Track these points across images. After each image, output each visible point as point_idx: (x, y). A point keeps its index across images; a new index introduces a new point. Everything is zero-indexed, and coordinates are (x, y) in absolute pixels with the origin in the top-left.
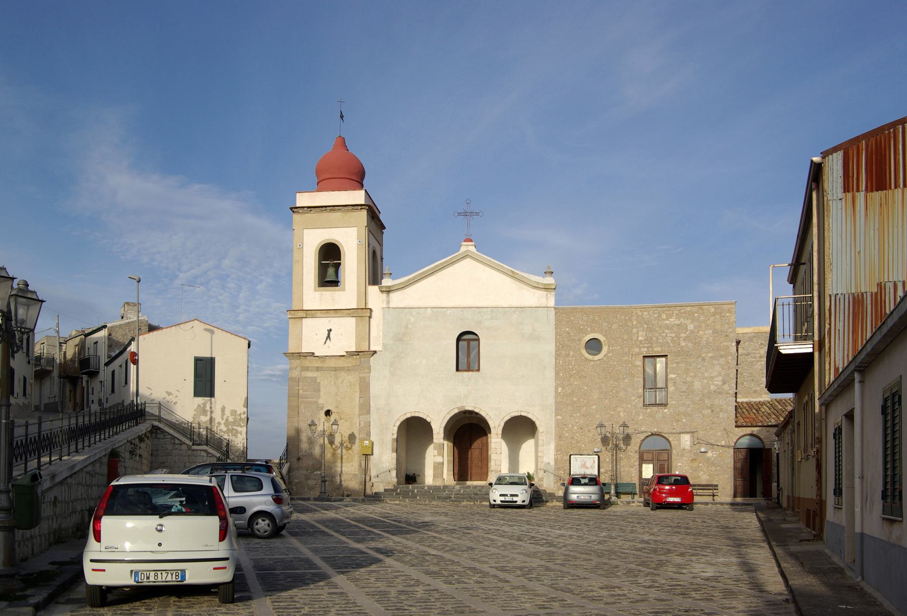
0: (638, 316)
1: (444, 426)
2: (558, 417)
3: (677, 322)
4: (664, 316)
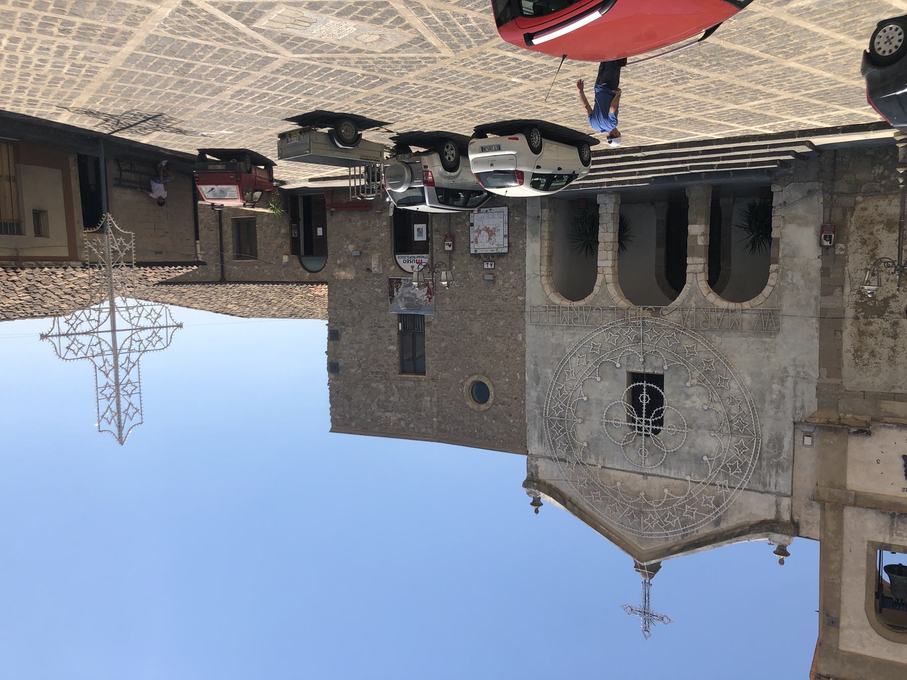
3: (388, 414)
4: (403, 423)
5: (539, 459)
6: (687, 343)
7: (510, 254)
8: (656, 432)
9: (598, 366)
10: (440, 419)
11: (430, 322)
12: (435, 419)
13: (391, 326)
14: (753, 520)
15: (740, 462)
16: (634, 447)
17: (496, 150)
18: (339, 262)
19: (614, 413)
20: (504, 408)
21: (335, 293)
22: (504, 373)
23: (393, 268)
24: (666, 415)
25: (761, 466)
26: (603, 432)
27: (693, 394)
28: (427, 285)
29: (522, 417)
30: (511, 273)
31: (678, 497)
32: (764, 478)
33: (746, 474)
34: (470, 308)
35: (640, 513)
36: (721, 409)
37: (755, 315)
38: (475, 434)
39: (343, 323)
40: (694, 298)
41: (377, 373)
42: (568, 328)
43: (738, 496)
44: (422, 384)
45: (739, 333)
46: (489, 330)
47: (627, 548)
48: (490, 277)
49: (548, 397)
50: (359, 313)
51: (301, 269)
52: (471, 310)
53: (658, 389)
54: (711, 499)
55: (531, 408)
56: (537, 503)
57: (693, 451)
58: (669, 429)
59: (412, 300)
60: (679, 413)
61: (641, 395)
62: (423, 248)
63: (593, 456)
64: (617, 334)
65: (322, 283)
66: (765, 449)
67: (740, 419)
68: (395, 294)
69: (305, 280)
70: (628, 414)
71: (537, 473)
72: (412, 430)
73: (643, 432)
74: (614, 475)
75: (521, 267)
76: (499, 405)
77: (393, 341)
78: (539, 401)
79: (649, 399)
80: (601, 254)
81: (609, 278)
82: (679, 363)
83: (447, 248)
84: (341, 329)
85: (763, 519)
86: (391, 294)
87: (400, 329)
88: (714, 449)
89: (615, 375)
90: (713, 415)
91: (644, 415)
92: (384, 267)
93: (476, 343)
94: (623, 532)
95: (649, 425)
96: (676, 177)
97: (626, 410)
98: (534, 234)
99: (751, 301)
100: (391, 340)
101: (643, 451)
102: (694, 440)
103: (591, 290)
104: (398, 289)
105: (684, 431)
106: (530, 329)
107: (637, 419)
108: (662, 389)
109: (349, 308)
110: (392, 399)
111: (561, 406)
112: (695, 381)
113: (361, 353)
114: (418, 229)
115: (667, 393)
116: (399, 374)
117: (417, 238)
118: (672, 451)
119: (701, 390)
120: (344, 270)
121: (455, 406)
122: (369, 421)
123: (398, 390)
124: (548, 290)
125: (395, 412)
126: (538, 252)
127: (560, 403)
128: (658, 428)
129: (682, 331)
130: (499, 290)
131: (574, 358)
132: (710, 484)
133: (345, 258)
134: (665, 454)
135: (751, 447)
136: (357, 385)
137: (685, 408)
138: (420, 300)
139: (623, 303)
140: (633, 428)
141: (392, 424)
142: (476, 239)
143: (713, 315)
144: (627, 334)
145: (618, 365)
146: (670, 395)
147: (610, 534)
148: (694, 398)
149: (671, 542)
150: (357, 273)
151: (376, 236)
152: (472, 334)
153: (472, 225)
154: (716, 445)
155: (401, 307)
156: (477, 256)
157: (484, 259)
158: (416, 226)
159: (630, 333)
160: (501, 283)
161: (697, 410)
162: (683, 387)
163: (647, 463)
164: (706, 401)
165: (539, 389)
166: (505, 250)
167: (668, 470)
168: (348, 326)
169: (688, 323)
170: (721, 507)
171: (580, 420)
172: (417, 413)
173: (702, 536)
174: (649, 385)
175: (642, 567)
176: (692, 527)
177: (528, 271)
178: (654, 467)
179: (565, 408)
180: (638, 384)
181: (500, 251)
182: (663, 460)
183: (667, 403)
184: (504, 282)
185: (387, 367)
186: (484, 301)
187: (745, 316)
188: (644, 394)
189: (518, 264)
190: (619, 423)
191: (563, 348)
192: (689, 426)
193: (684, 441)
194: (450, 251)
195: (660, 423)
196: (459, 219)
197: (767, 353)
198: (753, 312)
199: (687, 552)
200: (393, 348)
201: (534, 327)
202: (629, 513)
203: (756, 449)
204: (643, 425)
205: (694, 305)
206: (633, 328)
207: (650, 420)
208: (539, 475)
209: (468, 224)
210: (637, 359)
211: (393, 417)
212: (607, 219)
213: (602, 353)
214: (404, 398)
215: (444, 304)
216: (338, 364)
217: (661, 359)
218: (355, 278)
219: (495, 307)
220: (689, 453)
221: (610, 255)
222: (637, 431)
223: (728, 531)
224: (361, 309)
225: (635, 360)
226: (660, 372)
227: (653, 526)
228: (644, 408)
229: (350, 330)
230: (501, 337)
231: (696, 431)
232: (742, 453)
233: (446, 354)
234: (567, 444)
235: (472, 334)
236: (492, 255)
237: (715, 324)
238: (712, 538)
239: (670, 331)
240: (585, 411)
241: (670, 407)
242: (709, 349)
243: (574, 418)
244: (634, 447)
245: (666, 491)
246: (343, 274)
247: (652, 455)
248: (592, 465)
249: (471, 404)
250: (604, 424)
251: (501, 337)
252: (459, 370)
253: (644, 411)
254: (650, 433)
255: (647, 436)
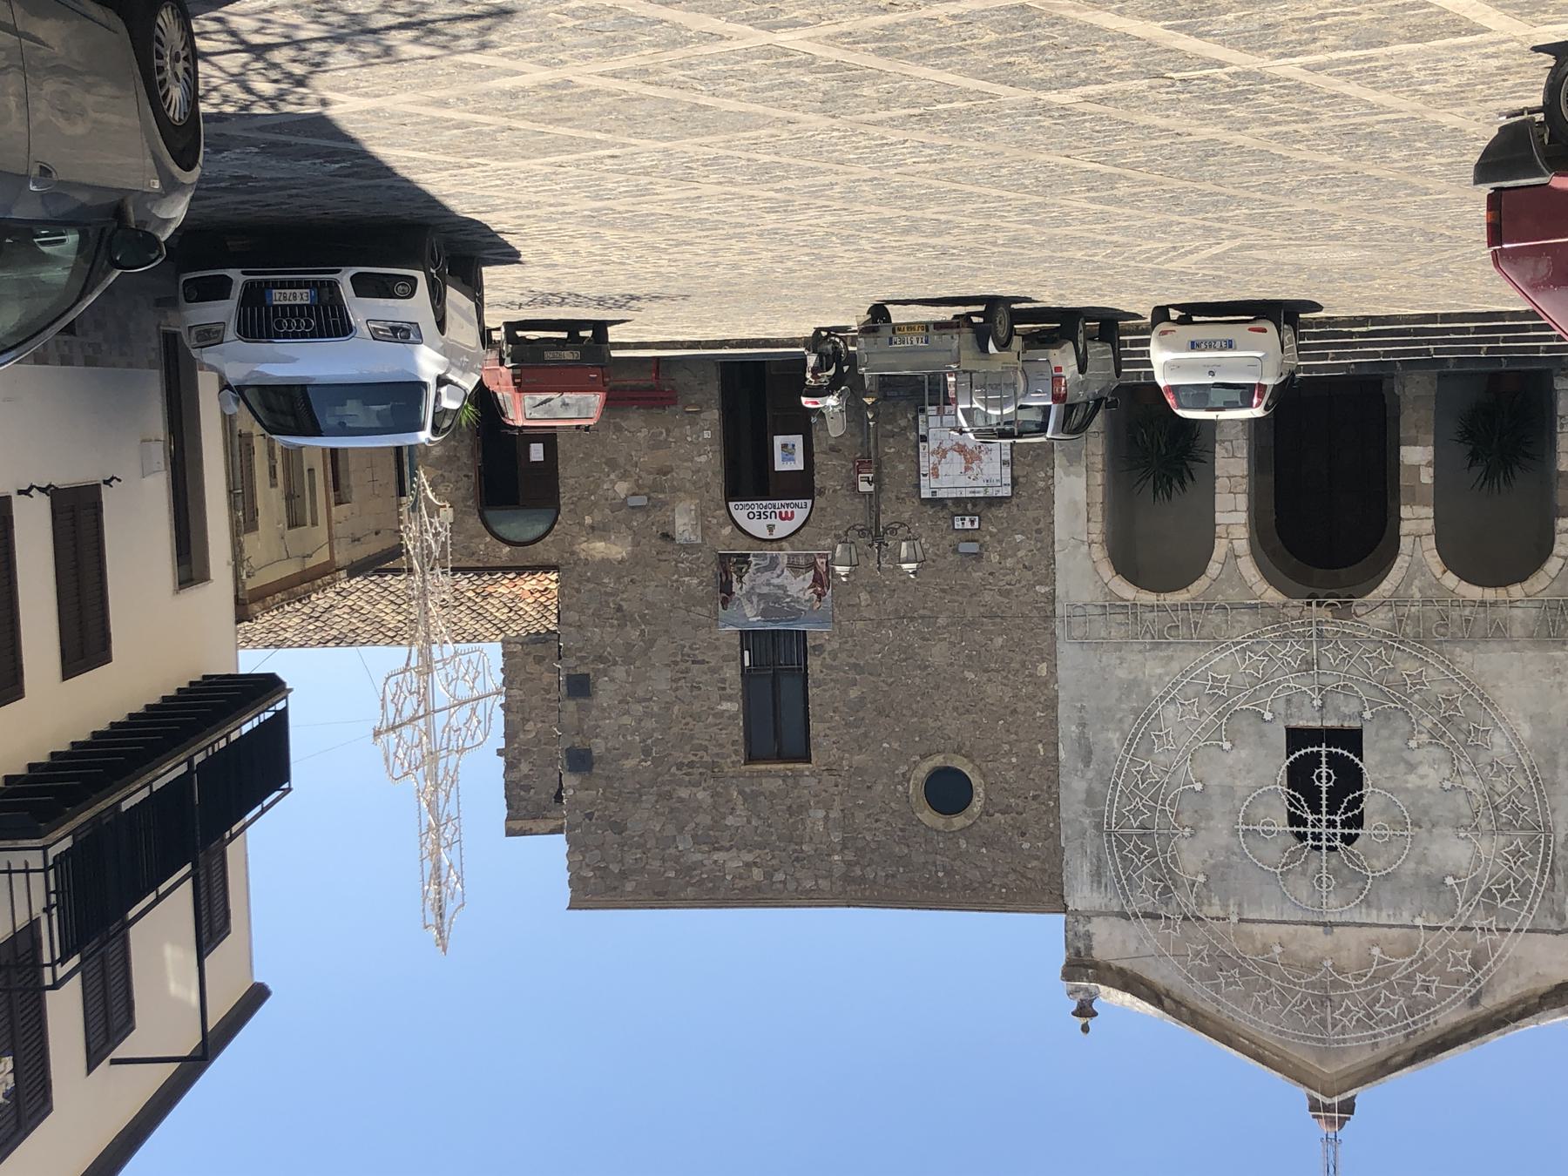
0: (829, 876)
1: (1398, 560)
2: (1047, 589)
3: (719, 856)
4: (757, 874)
5: (1095, 920)
6: (1408, 667)
7: (1014, 501)
8: (1349, 840)
9: (1224, 720)
10: (850, 856)
11: (822, 645)
12: (836, 858)
13: (725, 659)
14: (1544, 986)
15: (1516, 881)
16: (1304, 873)
17: (1221, 349)
18: (588, 520)
19: (1261, 811)
20: (1009, 819)
21: (578, 591)
22: (1006, 747)
23: (727, 530)
24: (1368, 806)
25: (1554, 885)
26: (1237, 850)
27: (1421, 762)
28: (813, 565)
29: (1054, 835)
30: (1019, 537)
31: (1401, 960)
32: (1559, 906)
33: (1528, 902)
34: (921, 612)
35: (1323, 1001)
36: (1477, 787)
37: (1534, 611)
38: (939, 882)
39: (601, 658)
40: (1416, 582)
41: (691, 765)
42: (1156, 646)
43: (1512, 945)
44: (804, 782)
45: (1505, 645)
46: (970, 657)
47: (1299, 1076)
48: (973, 548)
49: (1114, 789)
50: (643, 631)
51: (488, 539)
52: (922, 617)
53: (1352, 756)
54: (1464, 957)
55: (1073, 816)
56: (1085, 1010)
57: (1423, 869)
58: (1376, 832)
59: (778, 599)
60: (1394, 799)
61: (1317, 771)
62: (800, 486)
63: (1215, 900)
64: (1265, 655)
65: (546, 568)
66: (1558, 849)
67: (1514, 802)
68: (736, 587)
69: (497, 563)
70: (1292, 809)
71: (1089, 948)
72: (780, 886)
73: (1324, 843)
74: (1262, 934)
75: (1041, 525)
76: (997, 815)
77: (728, 691)
78: (1091, 798)
79: (1334, 778)
80: (1222, 500)
81: (1242, 546)
82: (1393, 705)
83: (864, 487)
84: (596, 671)
85: (1560, 982)
86: (726, 588)
87: (747, 663)
88: (1465, 864)
89: (1262, 735)
90: (1461, 798)
91: (1324, 809)
92: (705, 529)
93: (937, 687)
94: (1284, 1043)
95: (1335, 827)
96: (1398, 365)
97: (1287, 803)
98: (1073, 459)
99: (1526, 584)
100: (724, 689)
101: (1324, 879)
102: (1426, 848)
103: (1200, 571)
104: (741, 577)
105: (1405, 833)
106: (1068, 653)
107: (1310, 818)
108: (1360, 755)
109: (616, 622)
110: (730, 821)
111: (1143, 805)
112: (1425, 738)
113: (650, 724)
114: (784, 446)
115: (1370, 764)
116: (745, 764)
117: (780, 465)
118: (1384, 873)
119: (1437, 753)
120: (602, 539)
121: (888, 824)
122: (672, 874)
123: (745, 800)
124: (1107, 571)
125: (739, 850)
126: (1081, 495)
127: (1141, 799)
128: (1353, 831)
129: (1396, 645)
130: (991, 574)
131: (1172, 708)
132: (1462, 929)
133: (607, 511)
134: (1370, 881)
135: (1535, 852)
136: (641, 796)
137: (1407, 790)
138: (797, 601)
139: (1272, 595)
140: (1301, 837)
141: (729, 877)
142: (935, 468)
143: (1455, 614)
144: (1285, 655)
145: (1268, 716)
146: (1377, 766)
147: (1261, 1051)
148: (1423, 770)
149: (1383, 1051)
150: (636, 544)
151: (686, 461)
152: (926, 667)
153: (924, 439)
154: (1469, 853)
155: (752, 616)
156: (936, 502)
157: (953, 509)
158: (778, 440)
159: (1290, 651)
160: (995, 558)
161: (1430, 791)
162: (1402, 750)
163: (1333, 901)
164: (1447, 773)
165: (1090, 774)
166: (1007, 491)
167: (1374, 912)
168: (615, 663)
169: (1408, 629)
170: (1485, 968)
171: (1187, 830)
172: (793, 847)
173: (1447, 1030)
174: (1333, 750)
175: (1327, 1108)
176: (1427, 1017)
177: (1060, 533)
178: (1346, 908)
179: (1152, 809)
180: (1309, 750)
181: (991, 493)
182: (1365, 892)
183: (1370, 783)
184: (1003, 556)
185: (716, 750)
186: (955, 597)
187: (1517, 612)
188: (1324, 769)
189: (1034, 519)
190: (1272, 828)
191: (1144, 688)
192: (1416, 824)
193: (1406, 852)
194: (870, 494)
195: (1358, 821)
196: (889, 427)
197: (1559, 678)
198: (1530, 604)
199: (1422, 1063)
200: (733, 707)
201: (1077, 646)
202: (1301, 1003)
203: (1546, 855)
204: (1323, 830)
205: (1418, 596)
206: (1298, 642)
207: (1337, 819)
208: (1094, 953)
209: (912, 436)
210: (1307, 700)
211: (733, 861)
212: (1233, 431)
213: (1231, 693)
214: (759, 817)
215: (853, 606)
216: (589, 751)
217: (1357, 701)
218: (633, 555)
219: (982, 610)
220: (1416, 874)
221: (1242, 501)
222: (1310, 842)
223: (1498, 1012)
224: (648, 623)
225: (1303, 705)
226: (1355, 724)
227: (1354, 1023)
228: (1324, 796)
229: (620, 672)
230: (998, 671)
231: (1430, 831)
232: (1518, 863)
233: (861, 714)
234: (1160, 881)
235: (926, 667)
236: (974, 500)
237: (1461, 629)
238: (1470, 1028)
239: (1372, 645)
240: (1196, 812)
241: (1377, 790)
242: (1451, 676)
243: (1175, 828)
244: (1304, 873)
245: (1376, 951)
246: (599, 549)
247: (1343, 885)
248: (1218, 919)
249: (928, 816)
250: (1241, 833)
251: (998, 671)
252: (896, 745)
253: (1324, 803)
254: (1337, 843)
255: (1330, 849)
